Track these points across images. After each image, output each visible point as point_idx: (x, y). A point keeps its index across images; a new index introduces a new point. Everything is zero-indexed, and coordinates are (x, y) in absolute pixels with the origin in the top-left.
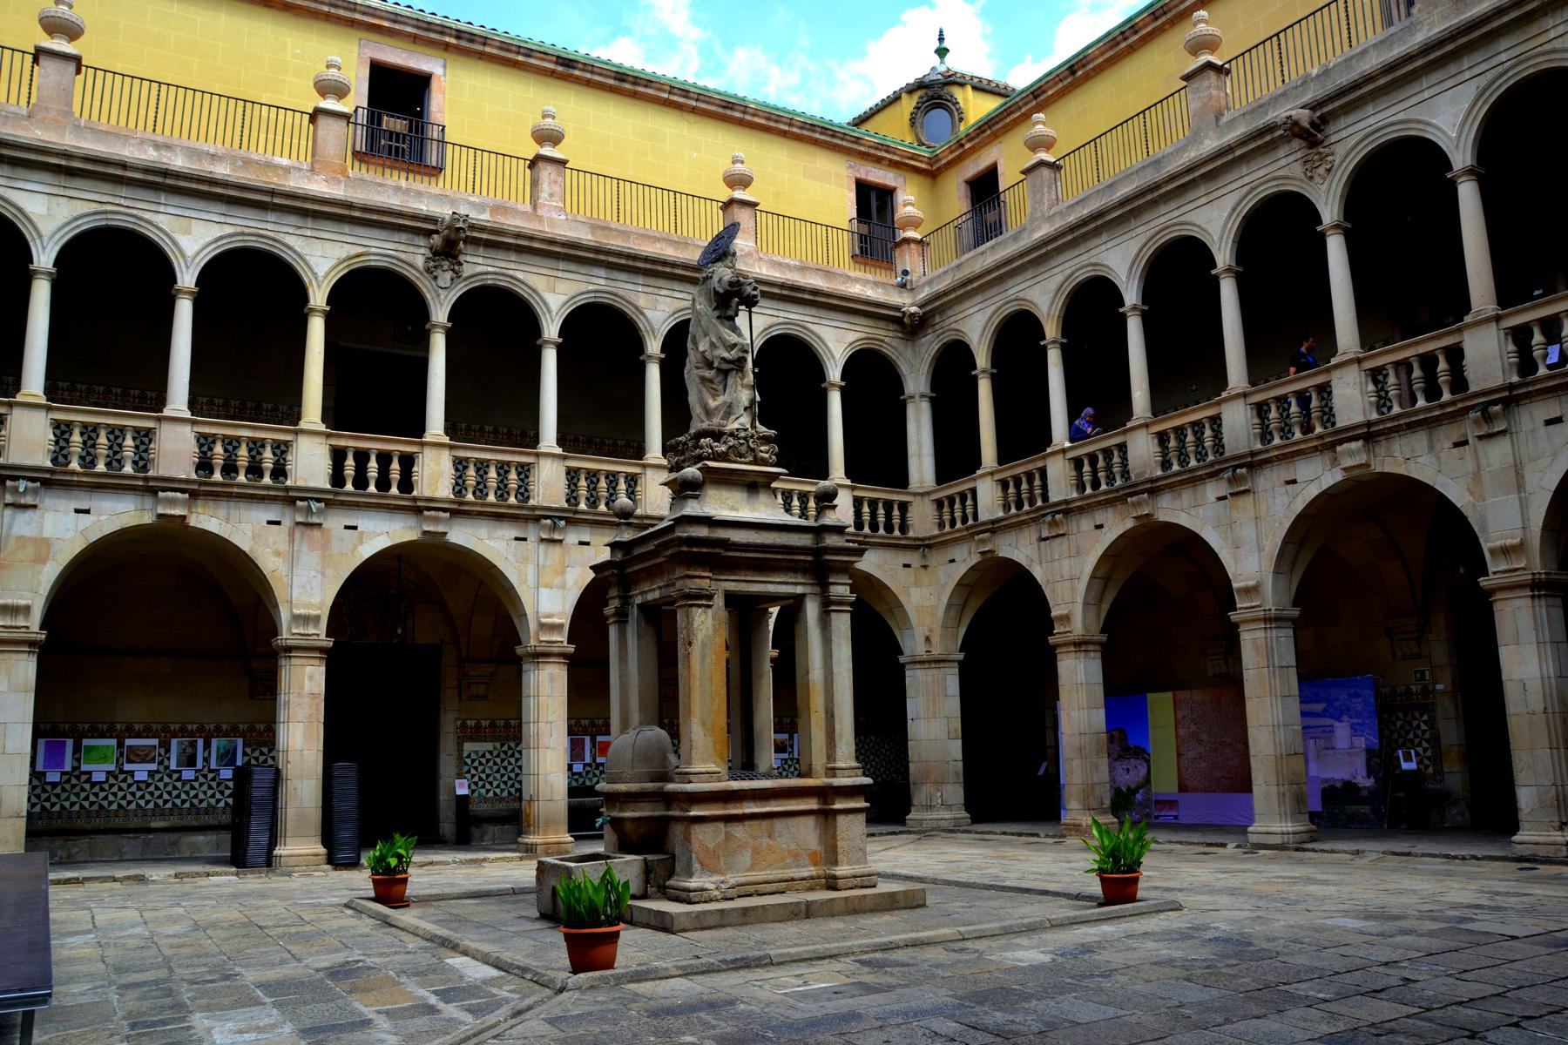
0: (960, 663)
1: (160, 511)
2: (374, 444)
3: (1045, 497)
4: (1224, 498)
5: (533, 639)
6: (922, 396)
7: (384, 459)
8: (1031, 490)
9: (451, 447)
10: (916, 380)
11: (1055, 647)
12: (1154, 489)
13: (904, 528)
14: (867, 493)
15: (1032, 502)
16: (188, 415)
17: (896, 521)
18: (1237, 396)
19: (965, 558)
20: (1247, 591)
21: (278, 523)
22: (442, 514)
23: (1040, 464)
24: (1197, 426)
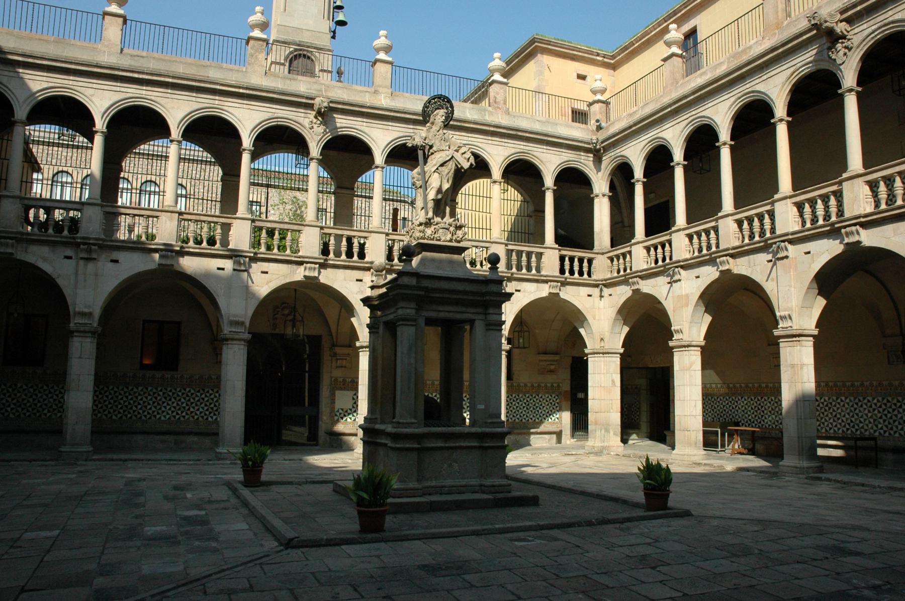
0: (621, 354)
2: (578, 253)
7: (581, 261)
9: (102, 206)
10: (600, 184)
11: (673, 348)
13: (538, 269)
14: (568, 252)
16: (99, 202)
17: (534, 265)
19: (623, 293)
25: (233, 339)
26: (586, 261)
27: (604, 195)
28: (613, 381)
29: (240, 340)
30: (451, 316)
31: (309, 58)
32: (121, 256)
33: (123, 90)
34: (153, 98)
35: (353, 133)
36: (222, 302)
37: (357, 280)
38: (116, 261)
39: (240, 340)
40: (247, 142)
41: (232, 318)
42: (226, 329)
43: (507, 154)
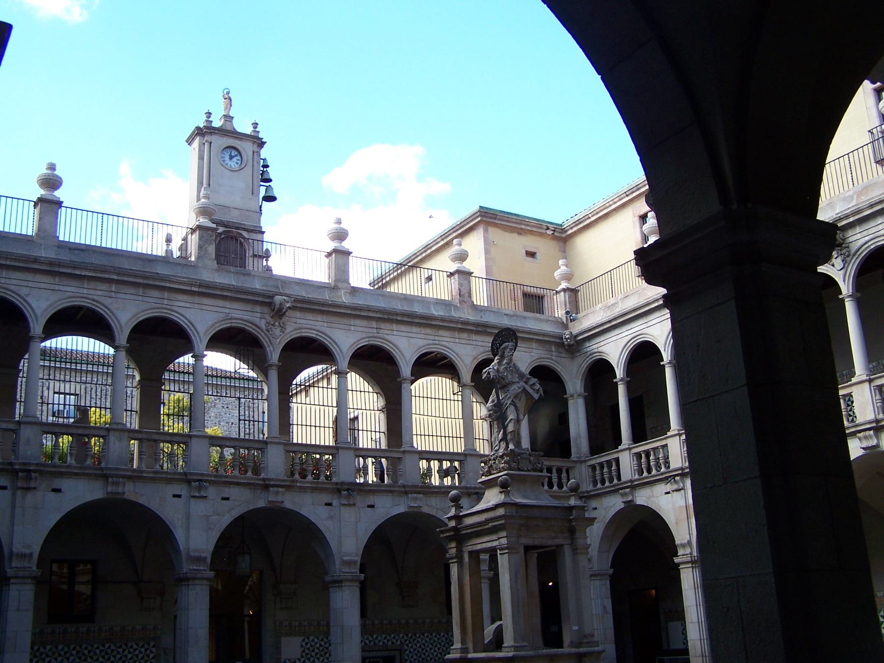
1: (109, 489)
3: (619, 479)
4: (668, 493)
5: (338, 569)
6: (572, 396)
8: (610, 472)
10: (574, 383)
11: (678, 564)
12: (634, 486)
15: (611, 481)
18: (626, 449)
20: (683, 546)
21: (179, 496)
22: (280, 489)
23: (615, 456)
24: (609, 462)
25: (195, 579)
26: (564, 471)
27: (572, 396)
28: (604, 607)
29: (202, 579)
30: (489, 545)
31: (241, 244)
32: (66, 484)
33: (62, 288)
34: (95, 297)
35: (312, 334)
36: (180, 535)
37: (327, 504)
38: (58, 491)
39: (202, 579)
40: (406, 370)
41: (192, 554)
42: (186, 567)
43: (475, 353)
